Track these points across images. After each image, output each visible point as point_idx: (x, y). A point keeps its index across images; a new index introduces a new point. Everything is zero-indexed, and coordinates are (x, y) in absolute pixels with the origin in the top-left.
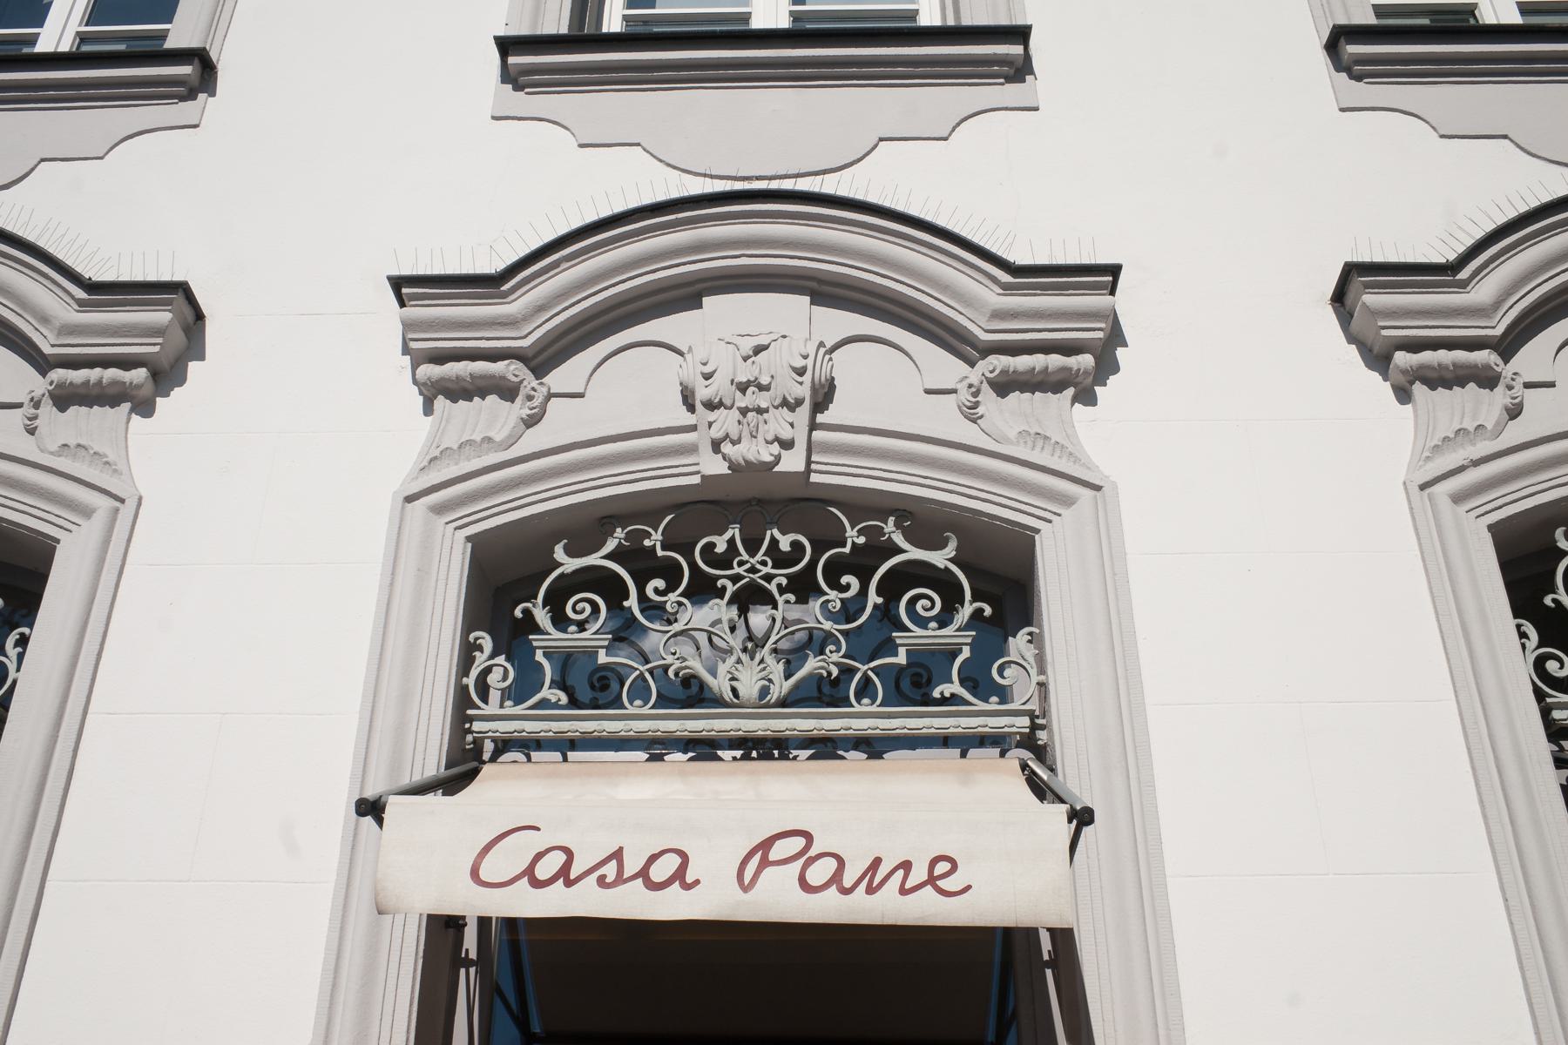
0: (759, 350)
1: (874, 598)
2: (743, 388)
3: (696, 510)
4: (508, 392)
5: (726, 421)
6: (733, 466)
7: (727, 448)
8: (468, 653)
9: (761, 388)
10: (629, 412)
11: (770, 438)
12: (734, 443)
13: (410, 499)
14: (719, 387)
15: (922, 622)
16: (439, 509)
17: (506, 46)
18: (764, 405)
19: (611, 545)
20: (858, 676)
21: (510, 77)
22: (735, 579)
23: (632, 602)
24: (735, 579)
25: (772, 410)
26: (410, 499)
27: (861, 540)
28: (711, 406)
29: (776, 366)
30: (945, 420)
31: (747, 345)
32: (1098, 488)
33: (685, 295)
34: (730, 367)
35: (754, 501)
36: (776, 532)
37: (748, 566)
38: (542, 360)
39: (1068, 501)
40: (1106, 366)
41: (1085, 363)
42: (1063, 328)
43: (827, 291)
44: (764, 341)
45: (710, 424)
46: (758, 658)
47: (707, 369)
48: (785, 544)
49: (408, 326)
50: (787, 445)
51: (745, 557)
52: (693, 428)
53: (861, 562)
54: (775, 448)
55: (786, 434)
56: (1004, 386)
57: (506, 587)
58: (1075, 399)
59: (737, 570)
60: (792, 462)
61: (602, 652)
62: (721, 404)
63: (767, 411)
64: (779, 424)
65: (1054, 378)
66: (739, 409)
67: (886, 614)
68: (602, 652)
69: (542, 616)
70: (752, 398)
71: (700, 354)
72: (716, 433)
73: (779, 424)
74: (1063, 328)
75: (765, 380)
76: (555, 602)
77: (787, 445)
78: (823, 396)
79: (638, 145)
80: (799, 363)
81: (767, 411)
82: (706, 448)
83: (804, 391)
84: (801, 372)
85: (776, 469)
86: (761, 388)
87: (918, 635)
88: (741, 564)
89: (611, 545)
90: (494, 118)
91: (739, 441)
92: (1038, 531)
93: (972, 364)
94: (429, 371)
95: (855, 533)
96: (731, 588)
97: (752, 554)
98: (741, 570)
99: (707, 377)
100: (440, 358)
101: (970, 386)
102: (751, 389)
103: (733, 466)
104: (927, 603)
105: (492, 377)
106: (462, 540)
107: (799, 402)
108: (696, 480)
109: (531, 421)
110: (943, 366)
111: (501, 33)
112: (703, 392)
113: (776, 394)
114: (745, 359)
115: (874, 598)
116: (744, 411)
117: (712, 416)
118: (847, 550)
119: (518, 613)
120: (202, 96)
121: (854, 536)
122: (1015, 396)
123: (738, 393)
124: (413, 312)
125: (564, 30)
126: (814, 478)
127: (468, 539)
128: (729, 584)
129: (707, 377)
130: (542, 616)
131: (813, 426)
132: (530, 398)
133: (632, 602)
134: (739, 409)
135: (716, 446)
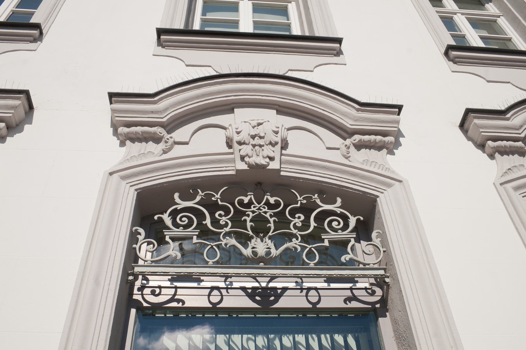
0: (259, 124)
1: (313, 224)
2: (253, 137)
3: (236, 184)
4: (157, 140)
5: (246, 150)
6: (249, 165)
7: (247, 159)
8: (133, 238)
9: (261, 138)
10: (204, 149)
11: (265, 156)
12: (249, 157)
13: (111, 174)
14: (244, 136)
15: (335, 230)
16: (123, 178)
17: (160, 32)
18: (262, 144)
19: (198, 198)
20: (308, 249)
21: (160, 43)
22: (253, 212)
23: (208, 221)
24: (253, 212)
25: (265, 146)
26: (111, 174)
27: (305, 201)
28: (240, 143)
29: (266, 130)
30: (336, 156)
31: (254, 123)
32: (400, 181)
33: (228, 108)
34: (246, 131)
35: (260, 180)
36: (269, 197)
37: (257, 208)
38: (172, 126)
39: (390, 186)
40: (397, 144)
41: (386, 141)
42: (377, 127)
43: (283, 110)
44: (261, 122)
45: (240, 150)
46: (264, 241)
47: (238, 130)
48: (272, 200)
49: (113, 111)
50: (272, 159)
51: (257, 204)
52: (232, 153)
53: (307, 210)
54: (267, 160)
55: (272, 155)
56: (359, 147)
57: (150, 212)
58: (388, 153)
59: (253, 209)
60: (274, 165)
61: (195, 237)
62: (244, 143)
63: (263, 146)
64: (268, 151)
65: (379, 145)
66: (252, 145)
67: (320, 229)
68: (195, 237)
69: (168, 221)
70: (257, 141)
71: (234, 126)
72: (243, 153)
73: (268, 151)
74: (377, 127)
75: (262, 135)
76: (174, 214)
77: (272, 159)
78: (285, 145)
79: (210, 66)
80: (276, 130)
81: (263, 146)
82: (238, 159)
83: (279, 139)
84: (277, 133)
85: (268, 168)
86: (261, 138)
87: (333, 235)
88: (254, 207)
89: (198, 198)
90: (153, 55)
91: (252, 157)
92: (378, 197)
93: (345, 139)
94: (122, 130)
95: (301, 199)
96: (251, 215)
97: (259, 204)
98: (255, 209)
99: (238, 133)
100: (129, 125)
101: (346, 146)
102: (257, 138)
103: (249, 165)
104: (336, 223)
105: (151, 133)
106: (134, 190)
107: (276, 143)
108: (233, 173)
109: (165, 152)
110: (331, 138)
111: (159, 27)
112: (236, 138)
113: (267, 139)
114: (253, 127)
115: (313, 224)
116: (254, 146)
117: (241, 147)
118: (299, 205)
119: (156, 217)
120: (39, 42)
121: (301, 200)
122: (363, 150)
123: (251, 140)
124: (116, 106)
125: (182, 27)
126: (282, 173)
127: (136, 190)
128: (251, 214)
129: (238, 133)
130: (168, 221)
131: (282, 154)
132: (166, 142)
133: (208, 221)
134: (252, 145)
135: (242, 158)
